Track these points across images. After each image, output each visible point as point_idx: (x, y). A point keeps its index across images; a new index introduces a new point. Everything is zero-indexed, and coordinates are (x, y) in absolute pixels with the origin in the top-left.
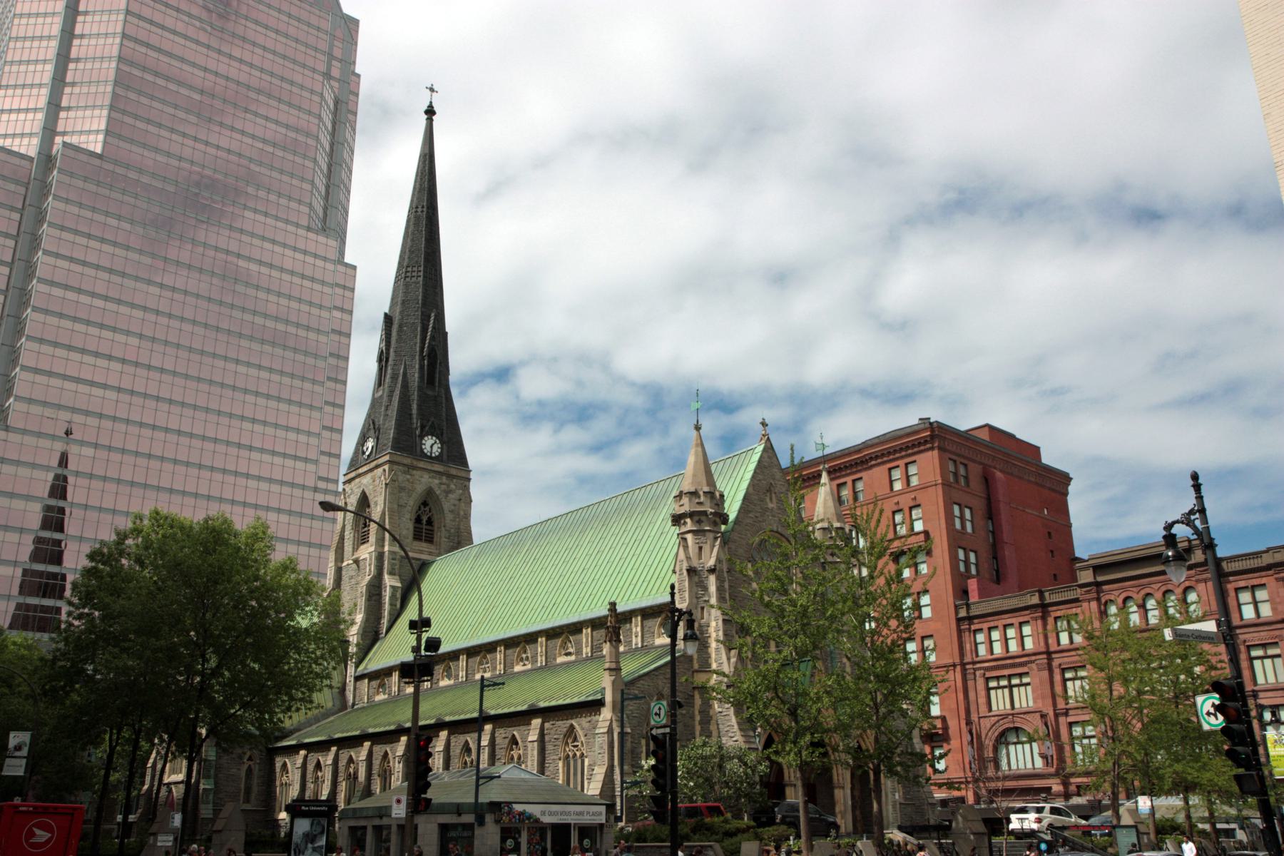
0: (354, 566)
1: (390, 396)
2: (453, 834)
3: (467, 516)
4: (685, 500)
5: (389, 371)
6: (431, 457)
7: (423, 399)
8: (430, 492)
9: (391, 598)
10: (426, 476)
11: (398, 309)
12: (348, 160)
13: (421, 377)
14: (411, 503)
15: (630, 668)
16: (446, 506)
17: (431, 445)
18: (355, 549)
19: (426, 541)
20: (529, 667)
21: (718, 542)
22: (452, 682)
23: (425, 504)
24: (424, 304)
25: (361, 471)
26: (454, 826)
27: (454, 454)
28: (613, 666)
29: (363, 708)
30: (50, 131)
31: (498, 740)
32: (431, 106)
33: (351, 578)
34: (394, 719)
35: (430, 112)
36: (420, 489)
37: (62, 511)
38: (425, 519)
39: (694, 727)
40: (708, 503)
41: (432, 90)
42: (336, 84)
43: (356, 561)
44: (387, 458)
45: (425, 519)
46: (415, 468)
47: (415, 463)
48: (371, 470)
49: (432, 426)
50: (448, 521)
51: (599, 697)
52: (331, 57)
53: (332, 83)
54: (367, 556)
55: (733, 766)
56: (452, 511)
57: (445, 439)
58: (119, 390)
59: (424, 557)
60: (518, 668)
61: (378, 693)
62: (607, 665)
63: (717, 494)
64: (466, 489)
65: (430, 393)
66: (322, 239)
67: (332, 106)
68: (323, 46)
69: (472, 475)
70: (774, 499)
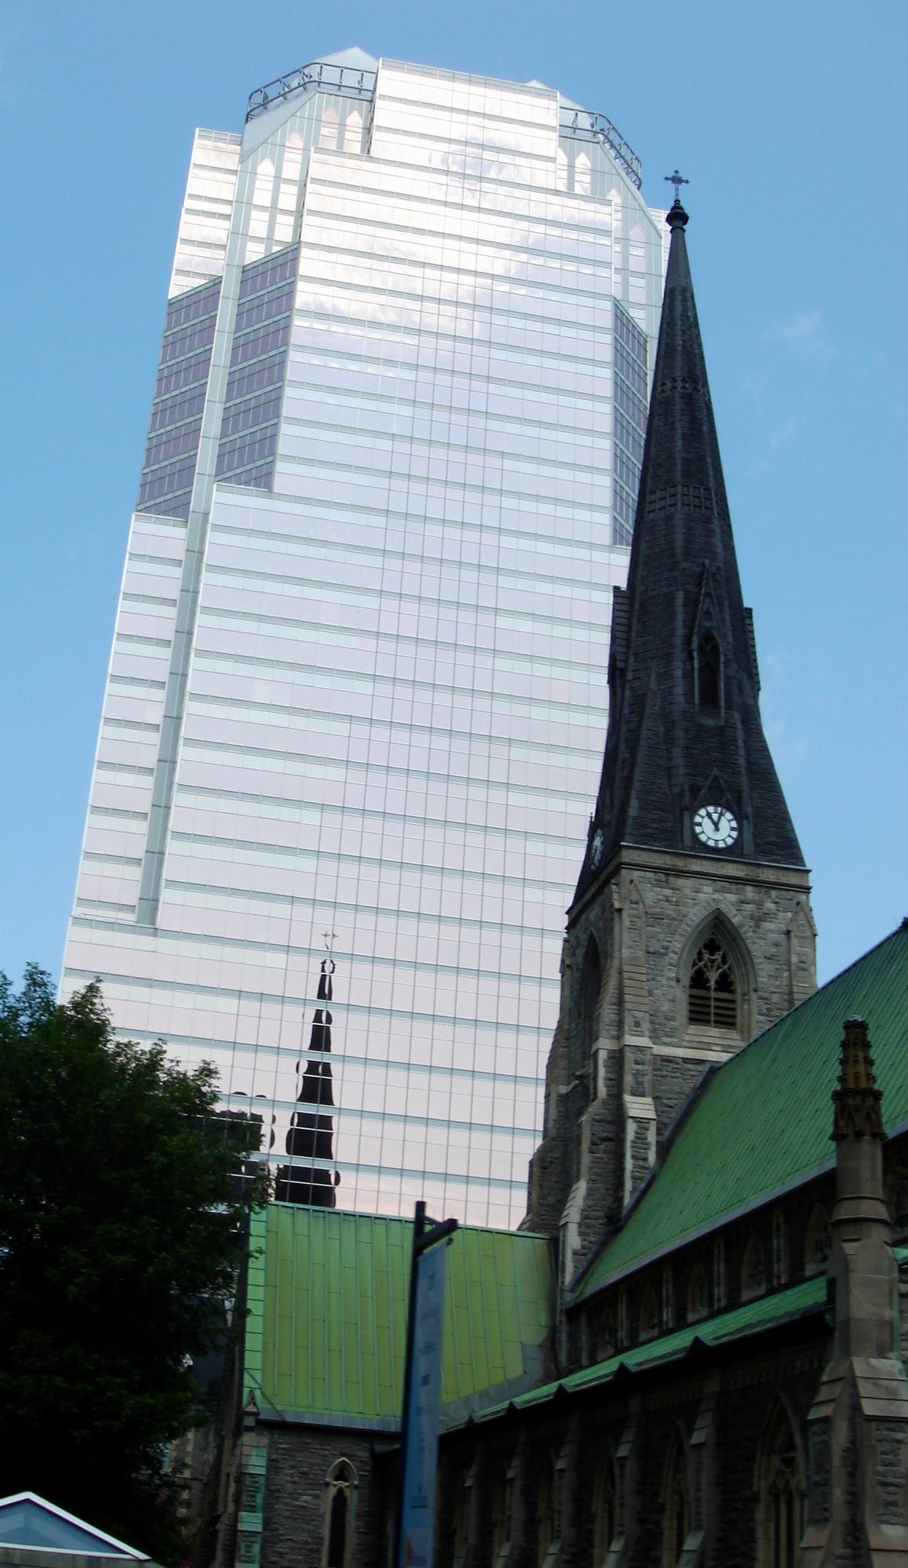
5: (628, 693)
6: (716, 850)
10: (708, 888)
13: (689, 694)
14: (677, 945)
23: (712, 946)
37: (326, 1122)
38: (713, 977)
41: (677, 180)
45: (713, 977)
47: (680, 863)
49: (716, 786)
50: (763, 979)
55: (145, 1472)
56: (769, 958)
64: (803, 911)
65: (710, 722)
69: (812, 880)
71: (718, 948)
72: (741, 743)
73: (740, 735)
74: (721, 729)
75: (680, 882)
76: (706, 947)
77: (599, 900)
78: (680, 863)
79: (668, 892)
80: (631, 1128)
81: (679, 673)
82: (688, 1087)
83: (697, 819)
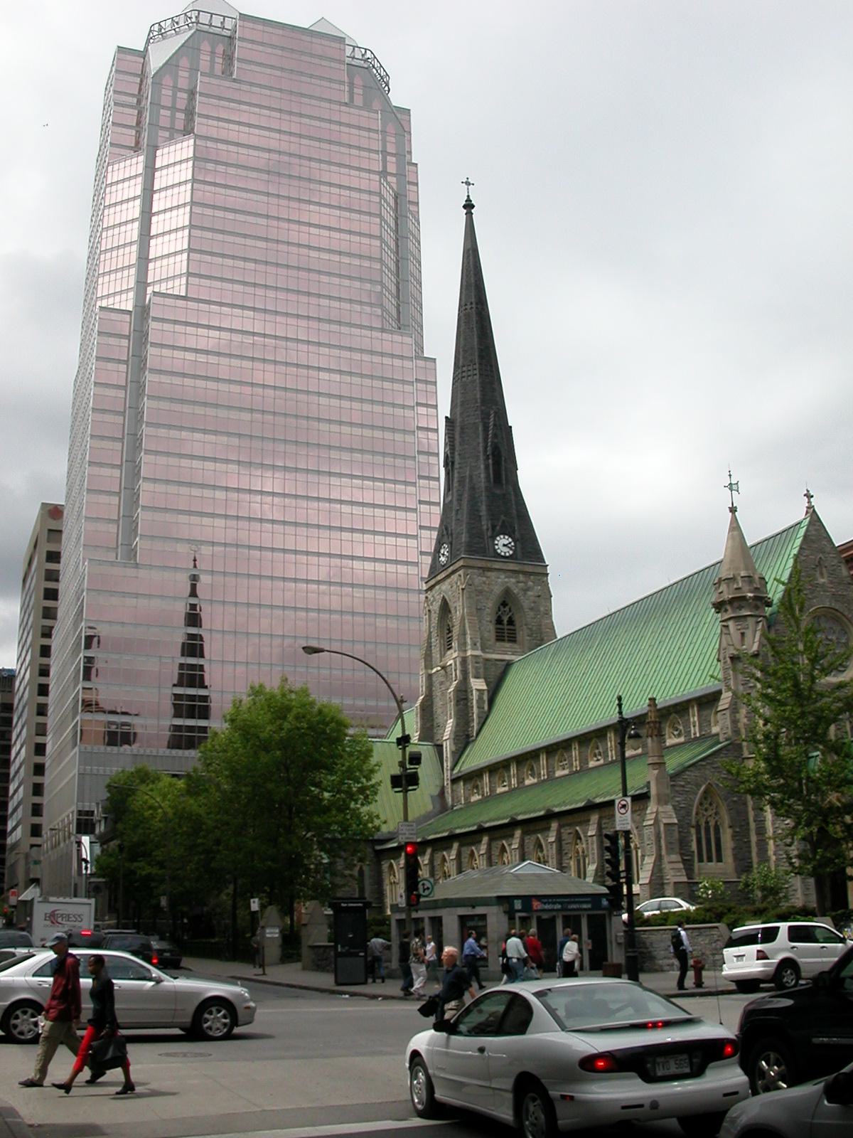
0: (442, 672)
1: (459, 500)
2: (471, 924)
3: (548, 613)
4: (723, 587)
5: (456, 475)
7: (492, 498)
8: (507, 592)
9: (477, 701)
11: (458, 410)
12: (415, 251)
13: (487, 477)
14: (490, 604)
15: (673, 762)
16: (526, 604)
17: (503, 544)
18: (443, 655)
19: (510, 641)
20: (602, 762)
21: (760, 626)
22: (536, 780)
23: (504, 604)
24: (483, 402)
25: (439, 578)
26: (471, 917)
27: (528, 548)
28: (656, 760)
29: (461, 809)
30: (142, 283)
31: (565, 836)
32: (468, 200)
33: (442, 683)
34: (471, 821)
35: (469, 206)
36: (498, 590)
38: (505, 619)
39: (747, 813)
40: (746, 588)
41: (468, 183)
42: (392, 179)
43: (444, 668)
44: (461, 563)
45: (505, 619)
46: (490, 570)
48: (448, 576)
49: (504, 526)
51: (645, 790)
52: (385, 153)
53: (389, 178)
54: (451, 662)
56: (531, 609)
57: (517, 535)
58: (226, 517)
59: (507, 657)
60: (592, 764)
61: (473, 794)
62: (650, 760)
63: (756, 577)
65: (498, 492)
66: (397, 338)
67: (392, 202)
68: (377, 146)
69: (549, 570)
70: (826, 575)
71: (507, 605)
72: (513, 502)
73: (513, 497)
74: (504, 495)
75: (489, 574)
76: (502, 604)
77: (449, 580)
78: (489, 565)
79: (484, 579)
80: (475, 695)
81: (482, 466)
82: (500, 670)
83: (496, 542)
